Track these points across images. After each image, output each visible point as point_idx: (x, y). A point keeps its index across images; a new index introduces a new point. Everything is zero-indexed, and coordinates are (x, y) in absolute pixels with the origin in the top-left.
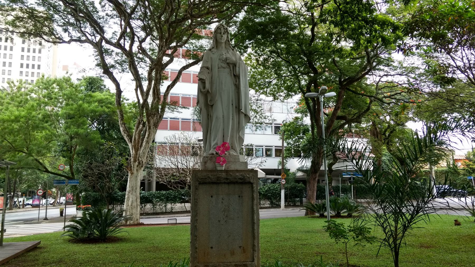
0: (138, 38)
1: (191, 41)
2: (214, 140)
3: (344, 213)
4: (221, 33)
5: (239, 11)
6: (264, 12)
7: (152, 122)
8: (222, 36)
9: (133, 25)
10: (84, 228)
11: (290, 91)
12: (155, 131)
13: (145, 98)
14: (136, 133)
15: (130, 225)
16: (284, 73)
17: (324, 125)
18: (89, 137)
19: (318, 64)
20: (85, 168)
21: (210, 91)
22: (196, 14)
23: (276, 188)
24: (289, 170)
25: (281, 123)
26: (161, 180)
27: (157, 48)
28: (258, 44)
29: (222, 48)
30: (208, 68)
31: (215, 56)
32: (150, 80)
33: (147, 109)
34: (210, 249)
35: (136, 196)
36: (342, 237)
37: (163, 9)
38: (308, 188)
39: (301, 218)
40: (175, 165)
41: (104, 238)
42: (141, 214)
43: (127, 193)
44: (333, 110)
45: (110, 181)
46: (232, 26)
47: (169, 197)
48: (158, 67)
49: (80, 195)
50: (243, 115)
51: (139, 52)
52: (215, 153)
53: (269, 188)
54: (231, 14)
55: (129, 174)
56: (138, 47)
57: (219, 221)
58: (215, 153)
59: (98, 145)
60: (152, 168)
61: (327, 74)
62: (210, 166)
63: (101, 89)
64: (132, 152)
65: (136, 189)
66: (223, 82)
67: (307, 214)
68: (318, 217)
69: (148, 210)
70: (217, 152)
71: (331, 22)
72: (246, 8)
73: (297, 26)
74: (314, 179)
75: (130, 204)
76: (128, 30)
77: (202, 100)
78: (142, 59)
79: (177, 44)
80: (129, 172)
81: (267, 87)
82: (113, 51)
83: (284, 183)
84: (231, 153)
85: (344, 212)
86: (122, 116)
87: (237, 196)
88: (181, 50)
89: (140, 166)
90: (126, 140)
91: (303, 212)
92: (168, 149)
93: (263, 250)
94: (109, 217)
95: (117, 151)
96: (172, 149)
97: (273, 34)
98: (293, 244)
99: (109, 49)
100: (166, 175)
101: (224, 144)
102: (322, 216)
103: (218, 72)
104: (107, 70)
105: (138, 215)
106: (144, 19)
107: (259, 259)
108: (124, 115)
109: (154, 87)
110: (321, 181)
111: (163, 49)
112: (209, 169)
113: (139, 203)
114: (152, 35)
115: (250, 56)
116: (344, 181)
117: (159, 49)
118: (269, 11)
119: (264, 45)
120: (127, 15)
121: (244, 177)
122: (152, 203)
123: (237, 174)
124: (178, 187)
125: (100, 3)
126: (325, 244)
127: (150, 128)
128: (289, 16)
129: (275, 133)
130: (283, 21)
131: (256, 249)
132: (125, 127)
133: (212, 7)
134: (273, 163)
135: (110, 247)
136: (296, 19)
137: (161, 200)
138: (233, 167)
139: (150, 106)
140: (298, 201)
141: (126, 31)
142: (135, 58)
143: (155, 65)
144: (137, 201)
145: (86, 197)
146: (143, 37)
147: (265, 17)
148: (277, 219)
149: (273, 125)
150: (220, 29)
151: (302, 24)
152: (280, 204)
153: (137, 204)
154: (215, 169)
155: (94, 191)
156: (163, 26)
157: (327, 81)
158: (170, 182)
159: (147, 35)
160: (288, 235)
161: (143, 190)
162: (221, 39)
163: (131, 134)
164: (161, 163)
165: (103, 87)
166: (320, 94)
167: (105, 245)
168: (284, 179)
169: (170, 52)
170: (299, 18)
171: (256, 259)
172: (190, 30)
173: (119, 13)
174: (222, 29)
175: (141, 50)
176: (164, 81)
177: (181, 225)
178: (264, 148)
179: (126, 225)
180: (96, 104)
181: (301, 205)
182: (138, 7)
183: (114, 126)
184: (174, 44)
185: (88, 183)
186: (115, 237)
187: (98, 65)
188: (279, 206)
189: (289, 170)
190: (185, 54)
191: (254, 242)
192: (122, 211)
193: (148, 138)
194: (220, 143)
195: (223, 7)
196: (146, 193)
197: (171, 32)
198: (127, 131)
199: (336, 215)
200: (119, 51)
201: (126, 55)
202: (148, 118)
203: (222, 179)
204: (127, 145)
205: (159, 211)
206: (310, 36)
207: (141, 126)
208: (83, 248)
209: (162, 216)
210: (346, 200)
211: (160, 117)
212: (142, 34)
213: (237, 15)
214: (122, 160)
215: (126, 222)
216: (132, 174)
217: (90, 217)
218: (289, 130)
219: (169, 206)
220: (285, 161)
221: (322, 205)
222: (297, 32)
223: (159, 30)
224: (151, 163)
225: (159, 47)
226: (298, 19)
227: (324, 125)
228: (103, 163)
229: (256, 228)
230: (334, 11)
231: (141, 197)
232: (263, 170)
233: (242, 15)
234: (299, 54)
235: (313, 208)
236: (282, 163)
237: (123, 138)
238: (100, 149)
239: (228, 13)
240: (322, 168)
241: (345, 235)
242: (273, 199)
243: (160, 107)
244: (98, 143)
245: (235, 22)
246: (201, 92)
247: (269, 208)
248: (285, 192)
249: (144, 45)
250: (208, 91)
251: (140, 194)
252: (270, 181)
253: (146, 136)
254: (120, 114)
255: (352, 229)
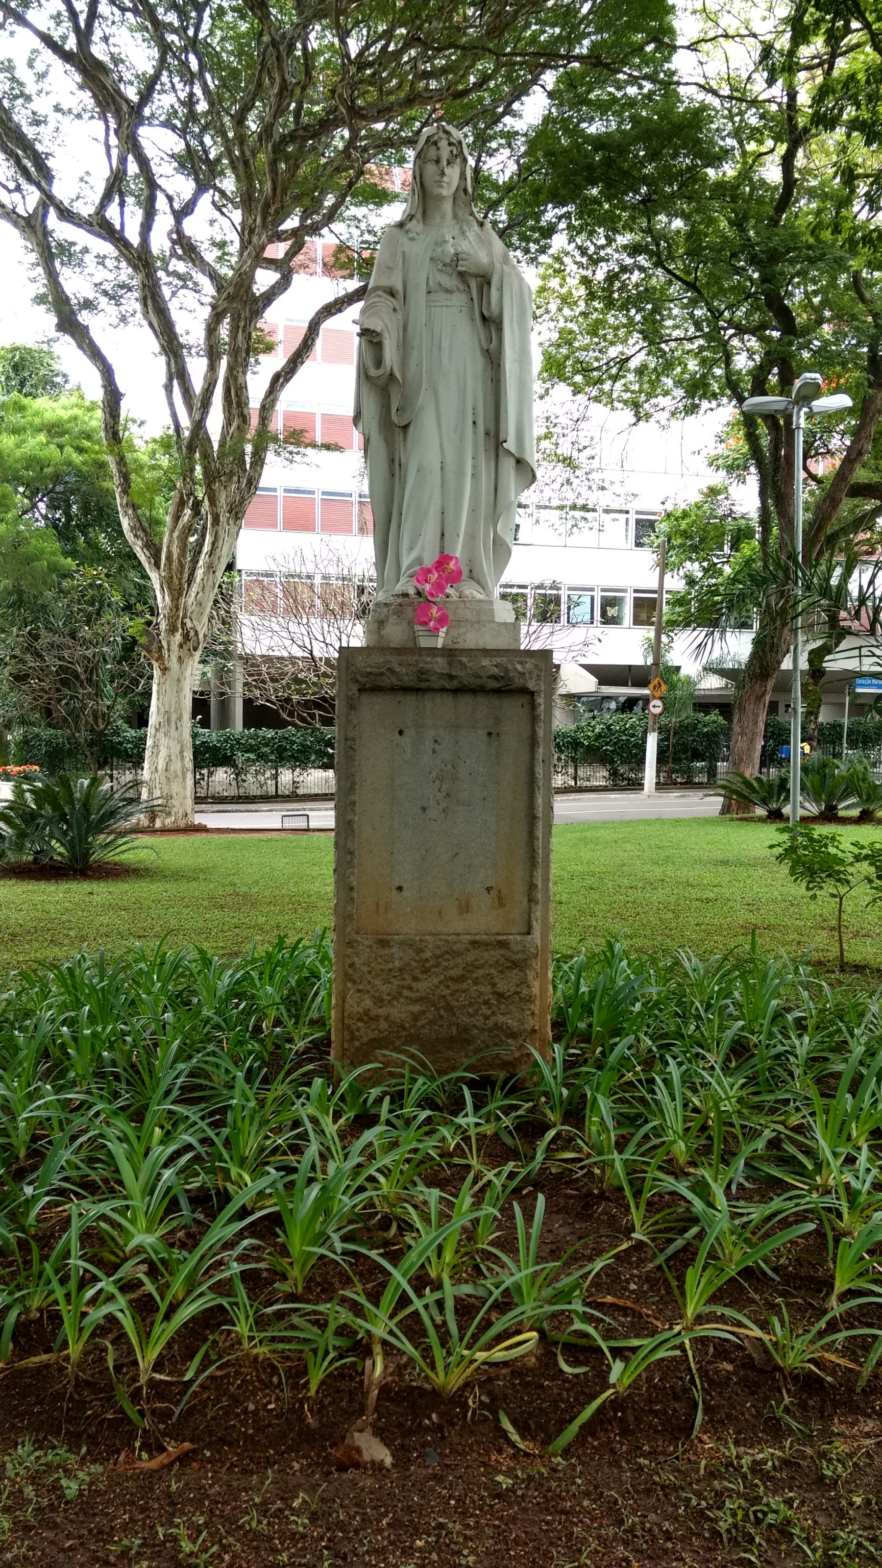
0: (170, 199)
1: (353, 211)
2: (411, 548)
3: (847, 808)
4: (438, 161)
5: (521, 91)
6: (619, 95)
7: (223, 499)
8: (443, 174)
9: (149, 151)
10: (22, 835)
11: (697, 390)
12: (234, 530)
13: (197, 417)
14: (171, 536)
15: (164, 831)
16: (676, 327)
17: (801, 517)
18: (22, 550)
19: (799, 295)
20: (17, 652)
21: (398, 375)
22: (369, 104)
23: (632, 727)
24: (678, 669)
25: (659, 508)
26: (258, 693)
27: (236, 239)
28: (591, 217)
29: (443, 217)
30: (392, 293)
31: (418, 249)
32: (213, 354)
33: (206, 456)
34: (394, 892)
35: (180, 742)
36: (829, 876)
37: (252, 87)
38: (736, 729)
39: (706, 821)
40: (303, 647)
41: (80, 867)
42: (198, 800)
43: (150, 730)
44: (838, 463)
45: (99, 694)
46: (497, 150)
47: (286, 749)
48: (239, 305)
49: (9, 737)
50: (512, 463)
51: (173, 254)
52: (412, 591)
53: (608, 727)
54: (495, 103)
55: (156, 673)
56: (169, 234)
57: (424, 809)
58: (412, 591)
59: (54, 576)
60: (227, 655)
61: (827, 329)
62: (395, 633)
63: (54, 385)
64: (162, 600)
65: (180, 718)
66: (445, 344)
67: (726, 810)
68: (761, 820)
69: (219, 789)
70: (420, 587)
71: (854, 125)
72: (549, 78)
73: (733, 148)
74: (760, 698)
75: (161, 765)
76: (133, 168)
77: (371, 411)
78: (184, 278)
79: (303, 219)
80: (155, 665)
81: (615, 378)
82: (86, 250)
83: (657, 711)
84: (467, 592)
85: (849, 808)
86: (125, 477)
87: (482, 733)
88: (321, 244)
89: (191, 645)
90: (142, 558)
91: (713, 803)
92: (280, 595)
93: (575, 912)
94: (95, 803)
95: (116, 598)
96: (294, 596)
97: (645, 180)
98: (672, 899)
99: (73, 244)
100: (273, 680)
101: (443, 560)
102: (775, 816)
103: (428, 307)
104: (69, 323)
105: (189, 802)
106: (185, 124)
107: (546, 929)
108: (133, 476)
109: (227, 380)
110: (781, 708)
111: (255, 239)
112: (393, 645)
113: (190, 765)
114: (216, 188)
115: (562, 263)
116: (860, 707)
117: (242, 240)
118: (632, 91)
119: (612, 225)
120: (125, 107)
121: (507, 670)
122: (235, 766)
123: (485, 662)
124: (312, 716)
125: (31, 64)
126: (775, 901)
127: (216, 520)
128: (704, 107)
129: (638, 544)
130: (679, 132)
131: (539, 896)
132: (138, 517)
133: (427, 75)
134: (627, 646)
135: (101, 891)
136: (731, 117)
137: (261, 757)
138: (471, 639)
139: (216, 446)
140: (701, 771)
141: (125, 172)
142: (161, 274)
143: (230, 298)
144: (182, 758)
145: (25, 743)
146: (187, 195)
147: (618, 114)
148: (629, 823)
149: (633, 517)
150: (435, 143)
151: (750, 138)
152: (642, 778)
153: (183, 766)
154: (411, 645)
155: (49, 725)
156: (254, 154)
157: (825, 359)
158: (288, 700)
159: (201, 188)
160: (658, 872)
161: (205, 724)
162: (439, 184)
163: (156, 541)
164: (257, 640)
165: (58, 380)
166: (796, 402)
167: (86, 886)
168: (660, 698)
169: (278, 250)
170: (741, 113)
171: (537, 926)
172: (346, 169)
173: (98, 103)
174: (443, 144)
175: (182, 248)
176: (262, 358)
177: (322, 834)
178: (598, 595)
179: (153, 831)
180: (42, 438)
181: (711, 783)
182: (164, 78)
183: (101, 513)
184: (291, 223)
185: (29, 699)
186: (116, 864)
187: (40, 300)
188: (636, 785)
189: (678, 669)
190: (331, 260)
191: (532, 876)
192: (137, 784)
193: (211, 553)
194: (429, 560)
195: (465, 76)
196: (211, 735)
197: (283, 179)
198: (144, 530)
199: (821, 813)
200: (107, 248)
201: (129, 263)
202: (209, 486)
203: (433, 678)
204: (146, 577)
205: (254, 791)
206: (776, 188)
207: (188, 512)
208: (20, 891)
209: (264, 807)
210: (859, 768)
211: (250, 483)
212: (181, 186)
213: (516, 106)
214: (134, 626)
215: (152, 820)
216: (165, 670)
217: (36, 801)
218: (690, 534)
219: (286, 776)
220: (664, 639)
221: (777, 782)
222: (729, 170)
223: (241, 167)
224: (225, 639)
225: (241, 235)
226: (737, 119)
227: (801, 517)
228: (73, 635)
229: (539, 833)
230: (868, 82)
231: (194, 746)
232: (591, 669)
233: (533, 109)
234: (734, 255)
235: (746, 792)
236: (656, 648)
237: (132, 556)
238: (61, 591)
239: (481, 99)
240: (786, 664)
241: (839, 872)
242: (617, 760)
243: (249, 448)
244: (54, 568)
245: (510, 136)
246: (367, 377)
247: (604, 789)
248: (660, 741)
249: (189, 226)
250: (391, 375)
251: (194, 736)
252: (613, 705)
253: (206, 548)
254: (120, 472)
255: (864, 852)
